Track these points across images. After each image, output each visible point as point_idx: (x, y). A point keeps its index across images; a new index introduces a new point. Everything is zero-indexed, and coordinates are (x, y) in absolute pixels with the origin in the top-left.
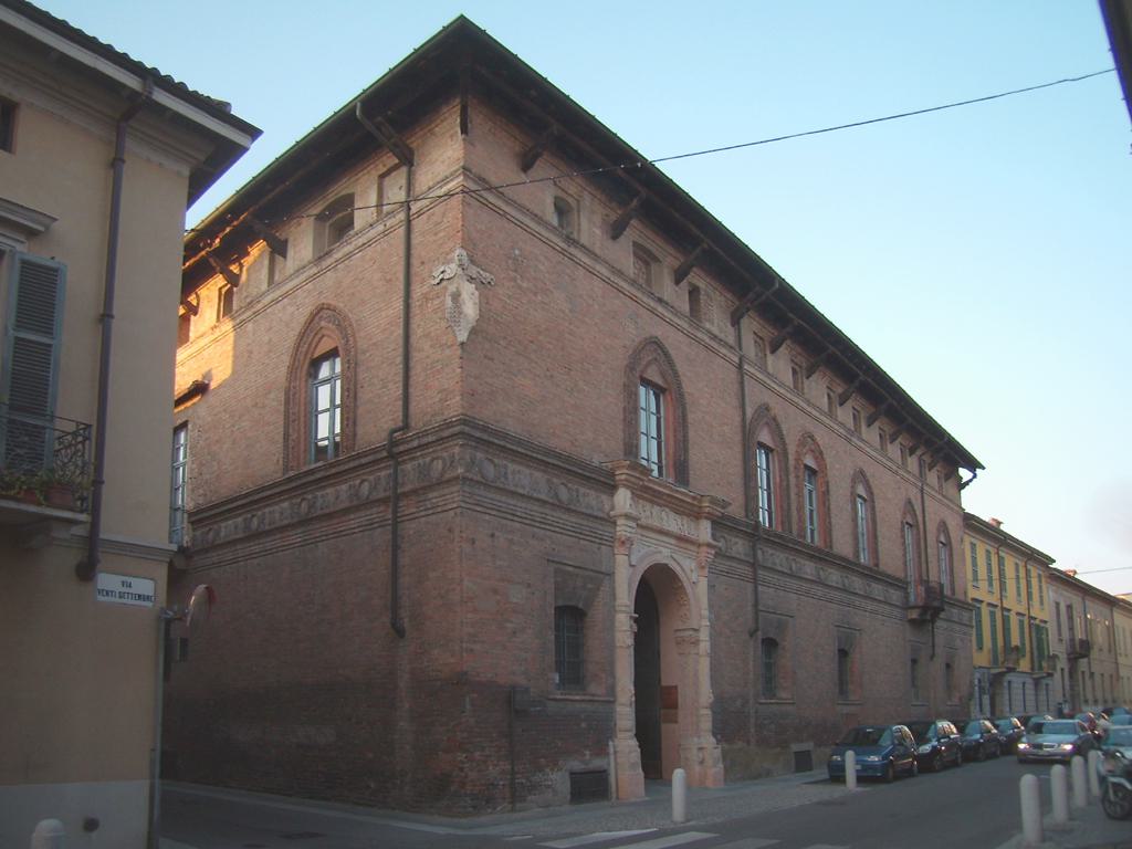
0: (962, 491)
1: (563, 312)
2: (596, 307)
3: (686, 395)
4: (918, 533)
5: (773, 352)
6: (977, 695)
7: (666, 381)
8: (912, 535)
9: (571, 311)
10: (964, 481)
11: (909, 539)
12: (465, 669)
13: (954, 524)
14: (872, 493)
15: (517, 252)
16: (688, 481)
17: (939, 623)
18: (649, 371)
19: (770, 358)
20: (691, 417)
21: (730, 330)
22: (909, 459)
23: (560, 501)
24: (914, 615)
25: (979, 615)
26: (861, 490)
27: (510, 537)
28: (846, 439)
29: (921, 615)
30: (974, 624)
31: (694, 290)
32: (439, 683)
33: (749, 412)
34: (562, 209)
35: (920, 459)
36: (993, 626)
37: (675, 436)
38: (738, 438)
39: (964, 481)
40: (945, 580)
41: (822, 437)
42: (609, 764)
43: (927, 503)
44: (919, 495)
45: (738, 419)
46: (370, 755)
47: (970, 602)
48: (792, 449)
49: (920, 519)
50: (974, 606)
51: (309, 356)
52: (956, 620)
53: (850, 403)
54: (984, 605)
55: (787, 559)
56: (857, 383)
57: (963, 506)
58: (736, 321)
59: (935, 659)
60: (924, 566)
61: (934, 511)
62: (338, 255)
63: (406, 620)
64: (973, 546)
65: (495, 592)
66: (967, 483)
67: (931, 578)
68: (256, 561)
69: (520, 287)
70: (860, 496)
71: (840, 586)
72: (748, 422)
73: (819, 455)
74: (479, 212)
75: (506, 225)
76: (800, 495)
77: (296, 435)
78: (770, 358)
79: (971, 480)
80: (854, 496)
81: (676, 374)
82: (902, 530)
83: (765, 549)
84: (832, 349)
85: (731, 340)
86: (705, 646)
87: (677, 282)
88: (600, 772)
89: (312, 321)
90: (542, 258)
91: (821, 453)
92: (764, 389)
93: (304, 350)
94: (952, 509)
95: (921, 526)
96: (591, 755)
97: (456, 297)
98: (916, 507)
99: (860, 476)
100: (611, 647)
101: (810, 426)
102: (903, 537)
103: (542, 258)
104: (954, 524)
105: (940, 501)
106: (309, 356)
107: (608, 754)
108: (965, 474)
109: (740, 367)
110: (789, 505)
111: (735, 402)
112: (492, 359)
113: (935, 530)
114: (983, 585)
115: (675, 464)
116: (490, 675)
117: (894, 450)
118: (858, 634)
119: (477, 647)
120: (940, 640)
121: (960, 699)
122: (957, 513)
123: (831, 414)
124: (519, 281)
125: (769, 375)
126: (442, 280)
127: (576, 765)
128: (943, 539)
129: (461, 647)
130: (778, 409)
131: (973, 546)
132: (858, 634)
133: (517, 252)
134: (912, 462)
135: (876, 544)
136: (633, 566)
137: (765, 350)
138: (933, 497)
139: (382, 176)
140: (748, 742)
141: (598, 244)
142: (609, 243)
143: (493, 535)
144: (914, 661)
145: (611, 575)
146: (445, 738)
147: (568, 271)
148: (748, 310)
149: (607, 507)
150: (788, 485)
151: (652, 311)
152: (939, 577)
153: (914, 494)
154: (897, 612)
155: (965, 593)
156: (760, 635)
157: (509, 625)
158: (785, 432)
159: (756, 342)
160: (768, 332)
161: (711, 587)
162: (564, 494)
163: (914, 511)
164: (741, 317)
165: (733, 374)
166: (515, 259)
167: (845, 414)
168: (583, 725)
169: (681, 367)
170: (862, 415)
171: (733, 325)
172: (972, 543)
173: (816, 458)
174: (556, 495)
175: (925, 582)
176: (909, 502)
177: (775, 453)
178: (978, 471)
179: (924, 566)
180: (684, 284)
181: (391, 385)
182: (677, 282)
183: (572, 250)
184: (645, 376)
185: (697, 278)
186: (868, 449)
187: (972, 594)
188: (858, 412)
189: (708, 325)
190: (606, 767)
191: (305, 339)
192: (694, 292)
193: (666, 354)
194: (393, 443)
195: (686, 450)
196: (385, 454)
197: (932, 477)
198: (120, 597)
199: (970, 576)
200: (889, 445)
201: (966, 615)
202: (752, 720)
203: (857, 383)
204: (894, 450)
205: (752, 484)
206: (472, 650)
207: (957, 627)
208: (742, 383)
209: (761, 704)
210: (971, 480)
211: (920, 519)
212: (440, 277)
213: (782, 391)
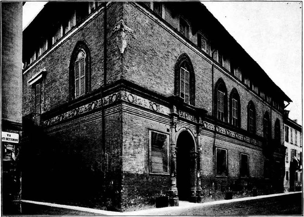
10: (285, 106)
36: (166, 119)
39: (285, 106)
55: (226, 130)
79: (288, 105)
83: (219, 127)
101: (235, 85)
108: (286, 103)
123: (243, 82)
125: (222, 68)
174: (152, 107)
178: (291, 103)
181: (101, 70)
198: (7, 140)
210: (288, 105)
213: (227, 73)
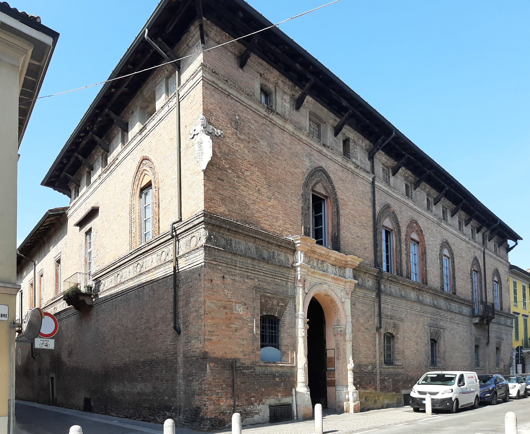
0: (509, 253)
1: (266, 153)
2: (286, 150)
3: (340, 200)
4: (481, 276)
5: (393, 175)
6: (514, 364)
7: (327, 192)
8: (477, 277)
9: (270, 152)
11: (475, 278)
12: (206, 350)
13: (503, 271)
14: (452, 254)
15: (237, 117)
16: (340, 248)
17: (491, 325)
18: (318, 186)
19: (392, 179)
20: (341, 212)
21: (369, 163)
22: (476, 235)
23: (435, 305)
24: (477, 321)
25: (517, 322)
26: (446, 252)
27: (234, 278)
28: (438, 224)
29: (480, 321)
30: (514, 325)
31: (346, 140)
32: (194, 358)
33: (378, 209)
34: (266, 93)
35: (483, 235)
37: (332, 223)
38: (371, 223)
39: (510, 247)
40: (497, 301)
41: (422, 223)
42: (292, 401)
43: (486, 259)
44: (482, 256)
45: (371, 213)
46: (166, 398)
47: (512, 313)
48: (404, 229)
49: (482, 268)
50: (514, 316)
51: (139, 186)
52: (503, 323)
53: (440, 205)
54: (521, 315)
56: (444, 192)
57: (509, 261)
58: (371, 158)
59: (490, 344)
60: (484, 294)
61: (492, 263)
62: (148, 128)
63: (181, 325)
64: (515, 283)
65: (225, 308)
66: (512, 248)
67: (488, 300)
68: (120, 298)
69: (239, 138)
70: (445, 256)
71: (432, 305)
72: (377, 214)
73: (420, 232)
74: (213, 93)
75: (231, 101)
76: (408, 255)
77: (135, 230)
78: (392, 179)
80: (441, 255)
81: (333, 187)
82: (471, 274)
84: (429, 172)
85: (368, 168)
86: (349, 336)
87: (336, 134)
88: (288, 405)
89: (139, 167)
90: (253, 122)
91: (422, 231)
92: (387, 196)
93: (137, 183)
94: (502, 263)
95: (483, 272)
96: (282, 396)
97: (200, 143)
98: (480, 262)
99: (445, 244)
100: (294, 338)
102: (471, 278)
103: (253, 122)
104: (503, 271)
105: (495, 259)
106: (139, 186)
107: (292, 395)
109: (373, 183)
110: (401, 261)
111: (370, 204)
112: (223, 180)
113: (491, 274)
114: (520, 304)
115: (332, 238)
116: (221, 354)
117: (468, 230)
118: (442, 330)
119: (214, 338)
120: (492, 335)
121: (504, 366)
122: (506, 265)
124: (238, 135)
126: (194, 135)
127: (272, 401)
128: (496, 279)
129: (204, 338)
130: (395, 207)
131: (515, 283)
132: (442, 330)
133: (237, 117)
134: (479, 237)
135: (455, 282)
136: (343, 302)
137: (389, 174)
138: (491, 256)
139: (168, 78)
140: (376, 389)
141: (287, 113)
142: (294, 112)
143: (224, 277)
144: (477, 347)
145: (294, 297)
146: (198, 388)
147: (268, 129)
148: (378, 150)
149: (291, 261)
150: (400, 250)
151: (320, 152)
152: (493, 300)
153: (479, 254)
154: (466, 319)
155: (509, 309)
156: (382, 331)
157: (233, 326)
158: (399, 220)
159: (383, 170)
160: (391, 162)
161: (353, 304)
162: (403, 294)
163: (479, 263)
164: (374, 154)
165: (369, 188)
166: (236, 122)
167: (438, 210)
168: (277, 379)
169: (337, 185)
170: (448, 210)
171: (369, 159)
172: (514, 282)
173: (418, 234)
175: (484, 303)
176: (476, 259)
177: (393, 231)
178: (518, 241)
179: (484, 294)
180: (340, 135)
182: (336, 134)
183: (271, 116)
184: (314, 189)
185: (348, 132)
186: (451, 230)
187: (513, 309)
188: (446, 209)
189: (354, 160)
190: (291, 402)
191: (137, 177)
192: (346, 142)
193: (328, 177)
194: (174, 229)
195: (339, 230)
196: (170, 237)
197: (491, 244)
199: (512, 299)
200: (464, 227)
201: (509, 321)
202: (378, 377)
203: (444, 192)
204: (468, 230)
205: (379, 249)
206: (211, 340)
207: (503, 327)
208: (374, 193)
209: (384, 368)
210: (514, 247)
211: (482, 268)
212: (193, 134)
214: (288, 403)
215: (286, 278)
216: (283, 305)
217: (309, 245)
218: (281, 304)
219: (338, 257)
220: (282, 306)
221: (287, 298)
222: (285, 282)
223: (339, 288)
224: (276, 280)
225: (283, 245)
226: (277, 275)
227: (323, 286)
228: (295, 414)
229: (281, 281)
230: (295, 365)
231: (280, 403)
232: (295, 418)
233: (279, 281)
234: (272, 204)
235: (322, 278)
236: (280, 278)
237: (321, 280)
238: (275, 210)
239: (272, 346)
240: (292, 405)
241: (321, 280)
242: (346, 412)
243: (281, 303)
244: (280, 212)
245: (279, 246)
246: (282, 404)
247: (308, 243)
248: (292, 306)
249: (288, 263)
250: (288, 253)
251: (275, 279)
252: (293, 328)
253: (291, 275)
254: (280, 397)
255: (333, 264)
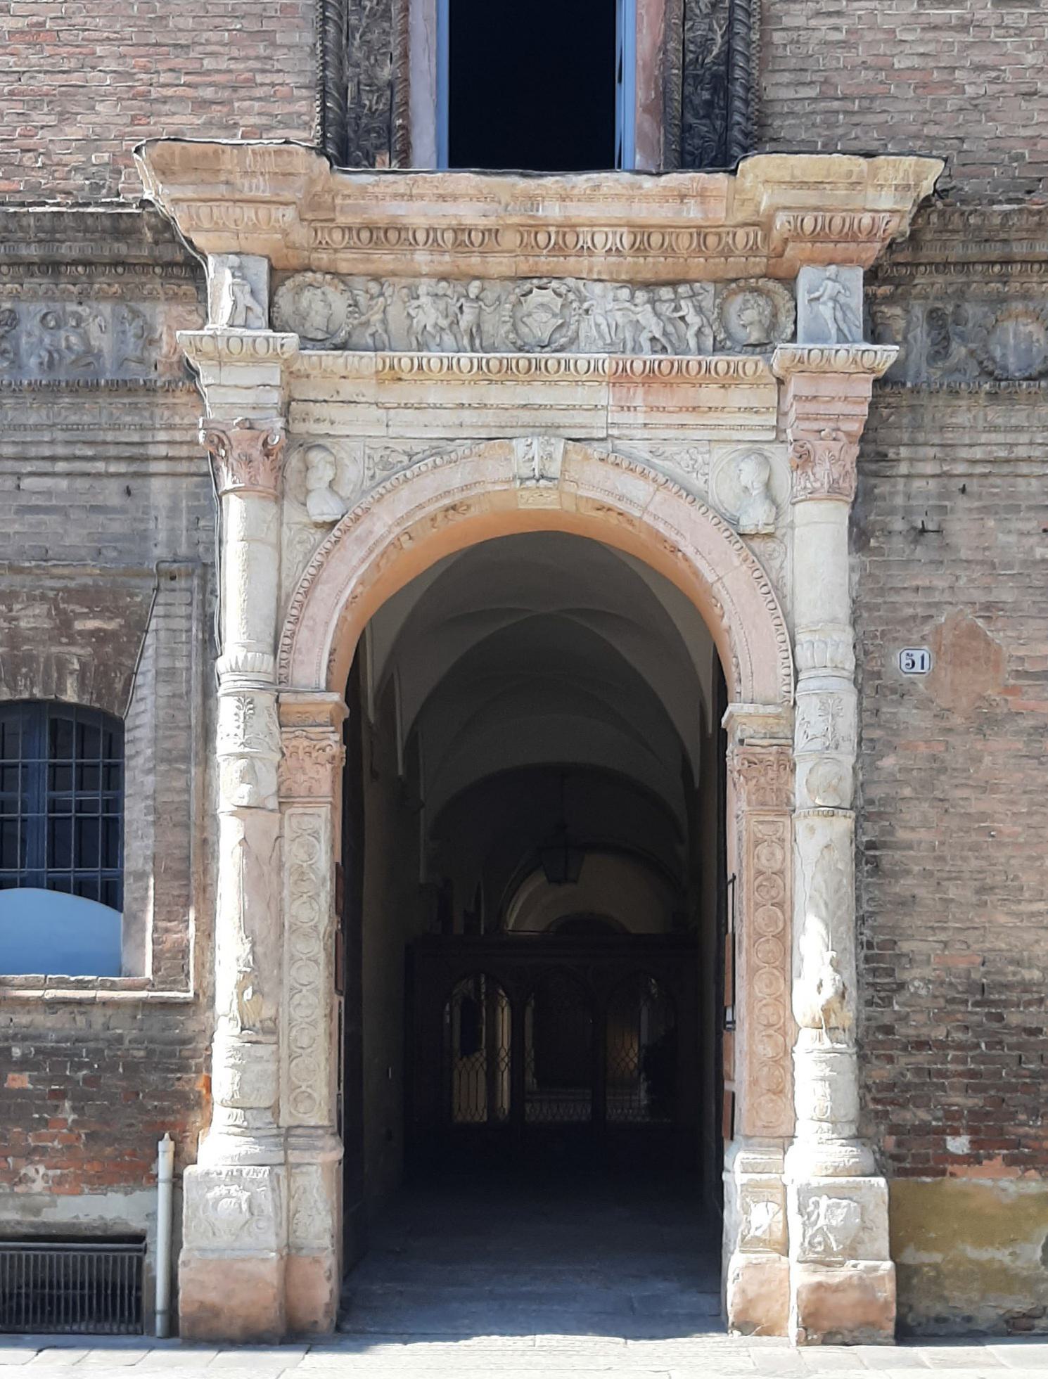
42: (152, 1216)
214: (120, 1229)
215: (118, 459)
216: (111, 626)
217: (267, 195)
218: (91, 624)
219: (660, 213)
220: (99, 637)
221: (135, 582)
222: (114, 486)
223: (715, 435)
224: (27, 483)
225: (68, 250)
226: (33, 451)
227: (512, 450)
228: (160, 1302)
229: (81, 484)
230: (191, 994)
231: (32, 1225)
232: (159, 1321)
233: (64, 484)
234: (21, 24)
235: (497, 395)
236: (61, 466)
237: (489, 417)
238: (48, 50)
239: (54, 886)
240: (148, 1240)
241: (489, 417)
242: (746, 1327)
243: (85, 616)
244: (99, 50)
245: (52, 267)
246: (43, 1232)
247: (238, 180)
248: (183, 624)
249: (141, 361)
250: (151, 297)
251: (19, 476)
252: (186, 759)
253: (171, 427)
254: (38, 1186)
255: (648, 275)
